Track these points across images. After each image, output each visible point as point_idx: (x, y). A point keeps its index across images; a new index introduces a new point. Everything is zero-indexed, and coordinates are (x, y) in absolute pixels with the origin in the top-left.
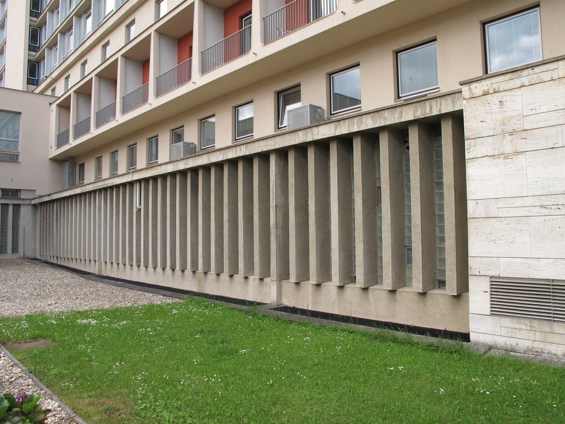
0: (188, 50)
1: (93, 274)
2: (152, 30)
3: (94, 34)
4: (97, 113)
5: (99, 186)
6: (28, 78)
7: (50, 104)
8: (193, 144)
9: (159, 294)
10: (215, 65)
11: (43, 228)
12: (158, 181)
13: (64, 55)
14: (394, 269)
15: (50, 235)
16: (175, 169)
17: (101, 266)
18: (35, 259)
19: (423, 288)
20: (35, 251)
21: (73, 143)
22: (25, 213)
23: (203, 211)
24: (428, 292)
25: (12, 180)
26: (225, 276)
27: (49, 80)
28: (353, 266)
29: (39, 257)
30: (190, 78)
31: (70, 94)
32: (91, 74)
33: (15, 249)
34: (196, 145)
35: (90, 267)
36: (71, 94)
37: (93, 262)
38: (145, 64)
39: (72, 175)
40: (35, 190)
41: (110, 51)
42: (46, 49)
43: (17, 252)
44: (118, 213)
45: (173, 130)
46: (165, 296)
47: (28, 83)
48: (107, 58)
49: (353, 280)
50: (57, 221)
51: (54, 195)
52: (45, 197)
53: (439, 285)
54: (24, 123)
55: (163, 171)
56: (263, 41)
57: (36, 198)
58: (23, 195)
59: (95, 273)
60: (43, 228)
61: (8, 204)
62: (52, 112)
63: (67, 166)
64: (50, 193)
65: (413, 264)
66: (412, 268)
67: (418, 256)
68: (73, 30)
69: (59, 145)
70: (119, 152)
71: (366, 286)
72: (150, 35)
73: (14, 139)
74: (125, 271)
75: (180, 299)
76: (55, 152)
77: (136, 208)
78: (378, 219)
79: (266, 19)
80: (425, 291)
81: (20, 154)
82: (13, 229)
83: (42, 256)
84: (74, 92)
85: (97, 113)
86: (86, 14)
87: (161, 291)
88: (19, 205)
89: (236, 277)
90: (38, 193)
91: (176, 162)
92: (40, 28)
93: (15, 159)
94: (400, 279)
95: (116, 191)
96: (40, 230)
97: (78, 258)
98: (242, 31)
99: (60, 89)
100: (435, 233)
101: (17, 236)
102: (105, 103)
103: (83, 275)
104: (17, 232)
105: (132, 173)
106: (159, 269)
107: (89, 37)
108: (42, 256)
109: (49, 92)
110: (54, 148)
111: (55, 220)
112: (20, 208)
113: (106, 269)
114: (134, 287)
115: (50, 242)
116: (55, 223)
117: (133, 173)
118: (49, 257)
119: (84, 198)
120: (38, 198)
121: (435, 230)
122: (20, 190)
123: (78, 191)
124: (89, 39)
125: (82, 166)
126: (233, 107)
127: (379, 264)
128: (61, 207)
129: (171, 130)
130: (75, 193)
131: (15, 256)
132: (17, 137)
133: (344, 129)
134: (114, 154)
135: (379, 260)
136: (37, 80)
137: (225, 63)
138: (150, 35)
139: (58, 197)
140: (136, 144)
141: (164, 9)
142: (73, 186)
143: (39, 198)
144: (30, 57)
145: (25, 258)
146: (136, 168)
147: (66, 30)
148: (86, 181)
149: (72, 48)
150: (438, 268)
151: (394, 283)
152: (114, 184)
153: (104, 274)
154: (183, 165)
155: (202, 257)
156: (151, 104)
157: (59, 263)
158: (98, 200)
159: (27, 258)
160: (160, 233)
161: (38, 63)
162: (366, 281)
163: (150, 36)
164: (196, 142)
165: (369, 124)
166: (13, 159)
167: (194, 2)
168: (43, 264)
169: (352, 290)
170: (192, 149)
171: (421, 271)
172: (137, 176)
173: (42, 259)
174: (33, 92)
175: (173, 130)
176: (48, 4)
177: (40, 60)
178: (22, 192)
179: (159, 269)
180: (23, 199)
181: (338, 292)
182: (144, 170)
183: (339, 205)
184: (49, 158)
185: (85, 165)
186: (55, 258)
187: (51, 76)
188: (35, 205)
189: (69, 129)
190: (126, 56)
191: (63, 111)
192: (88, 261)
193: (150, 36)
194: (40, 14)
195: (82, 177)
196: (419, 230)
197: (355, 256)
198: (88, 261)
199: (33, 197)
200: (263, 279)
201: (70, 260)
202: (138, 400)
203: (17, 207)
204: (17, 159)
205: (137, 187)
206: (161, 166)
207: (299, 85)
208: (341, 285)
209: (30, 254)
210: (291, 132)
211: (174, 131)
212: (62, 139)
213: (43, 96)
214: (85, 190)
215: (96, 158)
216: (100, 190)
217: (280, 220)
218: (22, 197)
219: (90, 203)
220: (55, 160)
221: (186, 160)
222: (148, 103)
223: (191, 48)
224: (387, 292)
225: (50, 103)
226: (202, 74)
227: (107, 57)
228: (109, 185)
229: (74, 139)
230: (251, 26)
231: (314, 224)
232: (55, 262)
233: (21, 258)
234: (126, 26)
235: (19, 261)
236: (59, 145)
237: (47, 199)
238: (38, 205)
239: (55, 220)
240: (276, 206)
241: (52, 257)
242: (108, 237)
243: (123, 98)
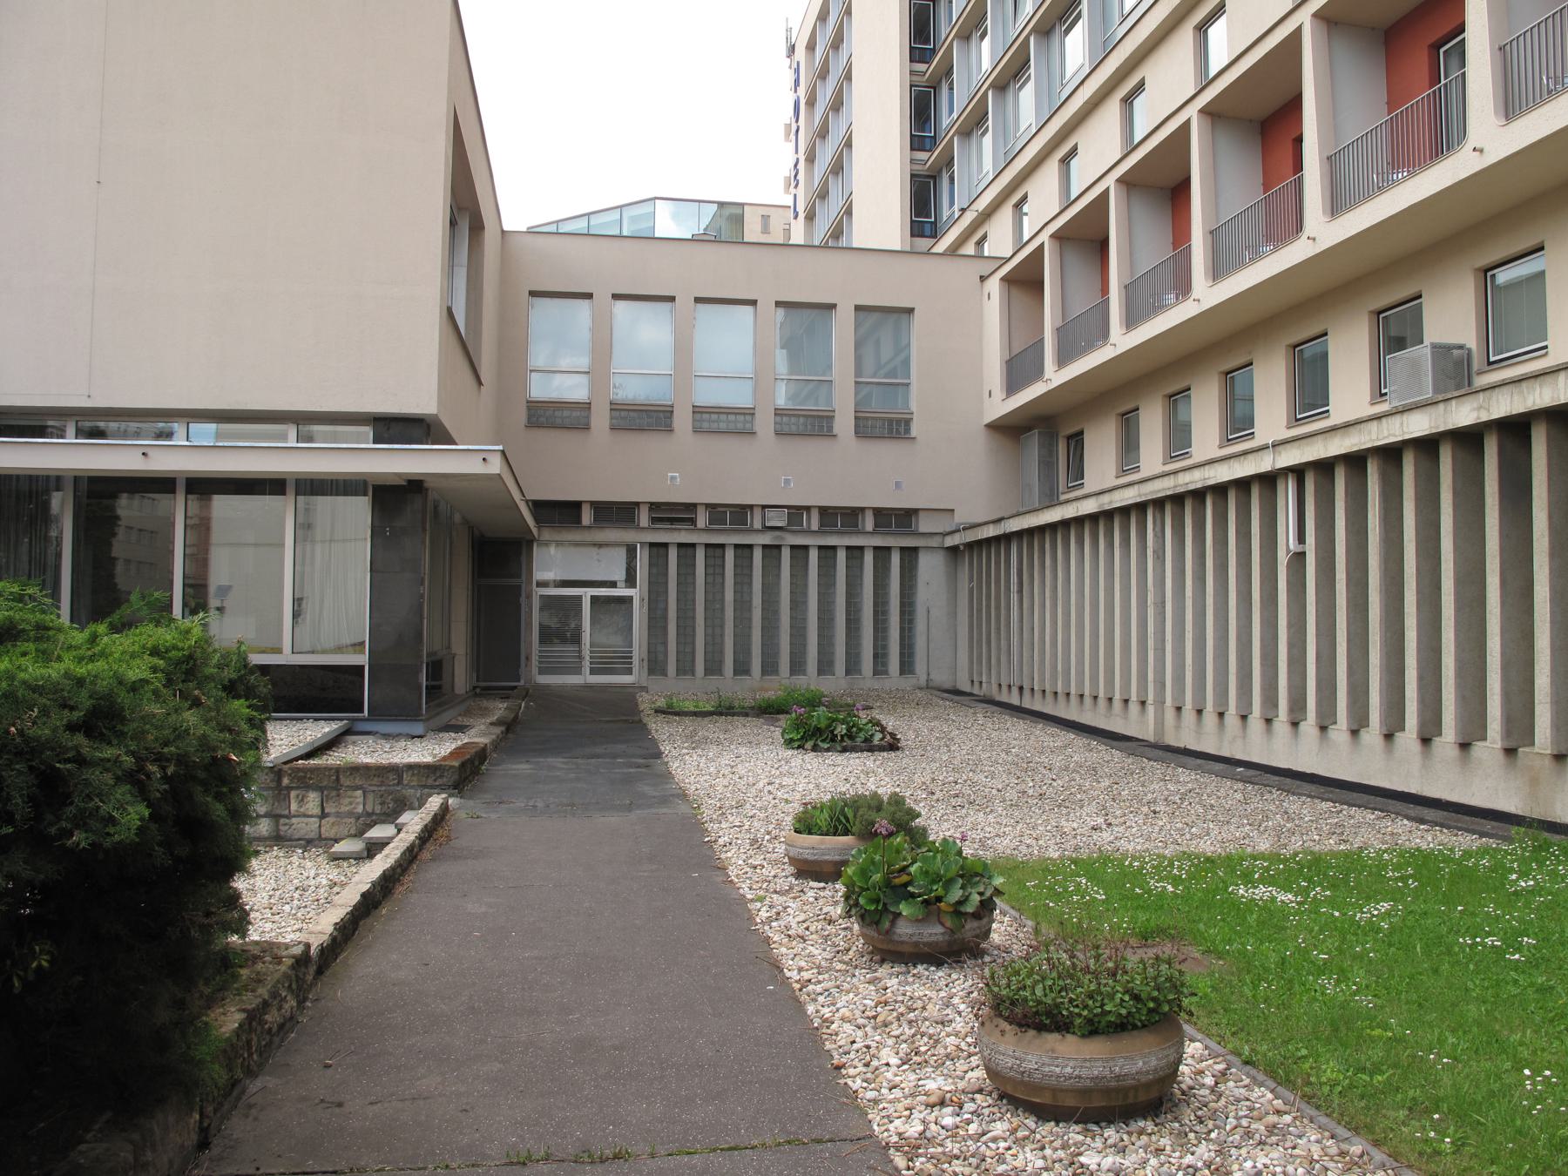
0: (1288, 148)
1: (1138, 740)
2: (1110, 181)
3: (1098, 70)
4: (1126, 287)
5: (1159, 491)
6: (912, 221)
7: (983, 279)
8: (1461, 347)
9: (1397, 814)
10: (1385, 175)
11: (979, 610)
12: (1369, 465)
13: (1005, 147)
15: (998, 629)
16: (1438, 427)
17: (1163, 719)
18: (957, 692)
20: (954, 668)
21: (1055, 376)
22: (930, 568)
23: (1553, 554)
24: (1397, 734)
25: (898, 485)
26: (1373, 734)
27: (969, 217)
29: (966, 688)
30: (1299, 227)
31: (1042, 245)
32: (1104, 179)
33: (907, 667)
34: (1469, 350)
35: (1126, 718)
36: (1043, 244)
37: (1134, 707)
38: (1178, 193)
39: (1048, 465)
40: (953, 510)
41: (1084, 171)
42: (956, 138)
43: (912, 672)
44: (1222, 567)
45: (1380, 313)
46: (1422, 821)
47: (912, 235)
48: (1073, 197)
50: (1020, 591)
51: (1011, 520)
52: (985, 528)
54: (919, 331)
55: (1390, 435)
56: (1211, 274)
57: (959, 531)
58: (925, 525)
59: (1141, 737)
60: (979, 610)
61: (889, 549)
62: (989, 298)
63: (1033, 443)
64: (999, 516)
68: (1032, 70)
69: (1012, 387)
70: (1192, 392)
72: (1188, 122)
73: (884, 378)
74: (1244, 737)
75: (1482, 835)
76: (1001, 406)
77: (1288, 550)
79: (1508, 47)
81: (915, 417)
82: (902, 613)
83: (976, 684)
84: (1201, 111)
85: (1126, 287)
86: (1065, 22)
87: (1399, 806)
88: (915, 549)
89: (1479, 749)
90: (961, 517)
91: (1441, 406)
92: (935, 89)
93: (902, 429)
95: (1214, 504)
96: (971, 616)
97: (1059, 690)
98: (1440, 89)
99: (1000, 240)
101: (910, 629)
102: (1081, 303)
103: (1115, 743)
104: (911, 621)
105: (1273, 446)
106: (1309, 725)
107: (1082, 82)
108: (976, 684)
109: (969, 249)
110: (999, 393)
111: (1014, 587)
112: (917, 557)
113: (1178, 727)
114: (1298, 787)
115: (999, 648)
116: (1014, 597)
117: (1277, 448)
118: (995, 687)
119: (1105, 525)
120: (964, 529)
122: (916, 511)
123: (1068, 512)
124: (1081, 88)
125: (1076, 440)
126: (1371, 312)
128: (1056, 548)
129: (1371, 312)
130: (1080, 513)
131: (907, 683)
132: (906, 363)
133: (1504, 406)
134: (1177, 399)
136: (935, 223)
137: (1431, 158)
138: (1188, 122)
139: (1026, 527)
140: (1251, 364)
141: (1222, 42)
142: (1052, 501)
143: (967, 532)
144: (916, 167)
145: (929, 687)
146: (1253, 433)
147: (1012, 74)
148: (1092, 482)
149: (988, 166)
152: (1211, 482)
153: (1171, 740)
154: (1471, 411)
155: (1548, 706)
156: (1314, 239)
157: (1027, 704)
158: (1154, 529)
159: (932, 688)
160: (1378, 625)
161: (934, 178)
163: (1106, 192)
164: (1470, 339)
165: (1264, 464)
166: (898, 432)
167: (1301, 26)
168: (986, 705)
170: (1458, 363)
172: (1195, 480)
173: (976, 691)
174: (928, 253)
175: (1380, 313)
176: (954, 21)
177: (940, 171)
178: (921, 514)
179: (1309, 725)
180: (924, 534)
182: (1319, 436)
184: (988, 420)
185: (1087, 438)
186: (1015, 691)
187: (974, 207)
188: (954, 550)
189: (1042, 340)
190: (1126, 182)
191: (1018, 294)
192: (1117, 704)
193: (1106, 192)
194: (934, 51)
195: (1077, 471)
198: (1117, 704)
199: (948, 529)
200: (1430, 740)
201: (1061, 698)
203: (910, 554)
204: (908, 430)
205: (1287, 494)
206: (1384, 420)
207: (1081, 433)
209: (942, 678)
210: (1514, 382)
211: (1297, 349)
212: (1020, 369)
213: (958, 258)
214: (1111, 502)
215: (1165, 396)
216: (1159, 503)
218: (922, 529)
219: (1110, 545)
220: (997, 427)
221: (1481, 394)
222: (1192, 299)
223: (1299, 140)
225: (981, 277)
226: (1214, 280)
227: (1137, 139)
228: (1192, 487)
229: (1127, 327)
230: (1464, 74)
232: (1015, 701)
233: (921, 689)
234: (1122, 100)
235: (920, 695)
236: (1012, 387)
237: (991, 532)
238: (962, 548)
239: (1014, 587)
241: (1004, 689)
242: (1189, 636)
243: (1211, 232)
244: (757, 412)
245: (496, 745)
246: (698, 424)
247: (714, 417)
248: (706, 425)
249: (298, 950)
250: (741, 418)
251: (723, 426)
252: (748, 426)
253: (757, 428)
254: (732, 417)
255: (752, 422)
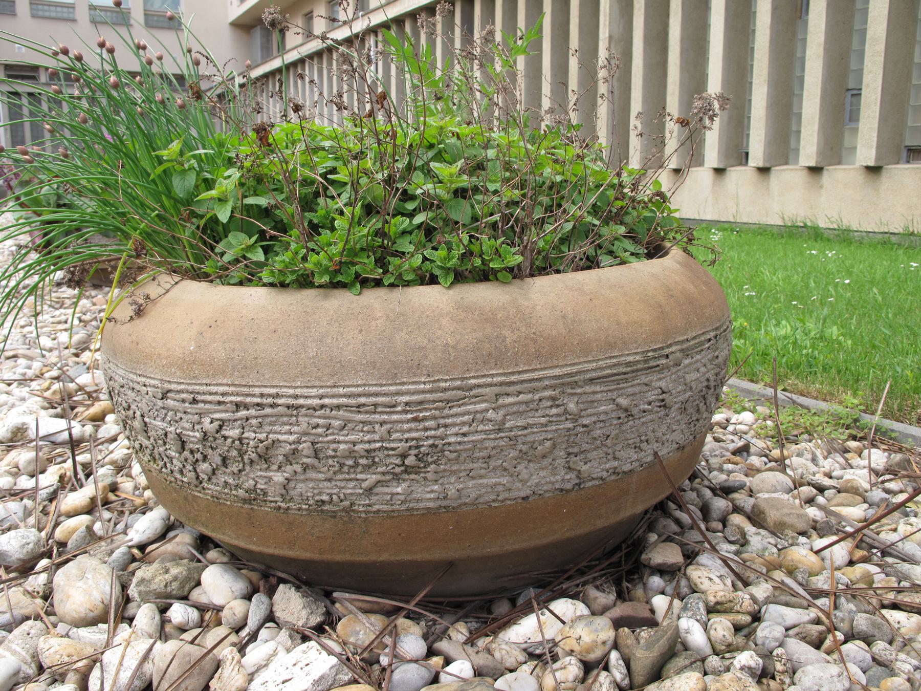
14: (823, 128)
19: (878, 158)
28: (745, 136)
49: (743, 158)
53: (908, 157)
63: (258, 33)
65: (860, 124)
66: (857, 129)
67: (874, 97)
71: (767, 165)
78: (799, 45)
80: (879, 164)
94: (832, 149)
100: (912, 59)
121: (913, 53)
123: (276, 63)
127: (794, 128)
135: (794, 120)
142: (267, 56)
148: (289, 44)
150: (909, 124)
151: (820, 153)
162: (768, 155)
169: (740, 177)
171: (876, 126)
181: (714, 182)
183: (726, 20)
196: (881, 47)
197: (749, 118)
202: (425, 117)
208: (721, 166)
217: (617, 53)
224: (805, 172)
231: (678, 62)
240: (610, 37)
244: (76, 6)
245: (728, 514)
246: (35, 12)
247: (46, 8)
248: (41, 13)
249: (586, 629)
250: (65, 10)
251: (53, 15)
252: (71, 16)
253: (77, 17)
254: (59, 9)
255: (73, 13)
